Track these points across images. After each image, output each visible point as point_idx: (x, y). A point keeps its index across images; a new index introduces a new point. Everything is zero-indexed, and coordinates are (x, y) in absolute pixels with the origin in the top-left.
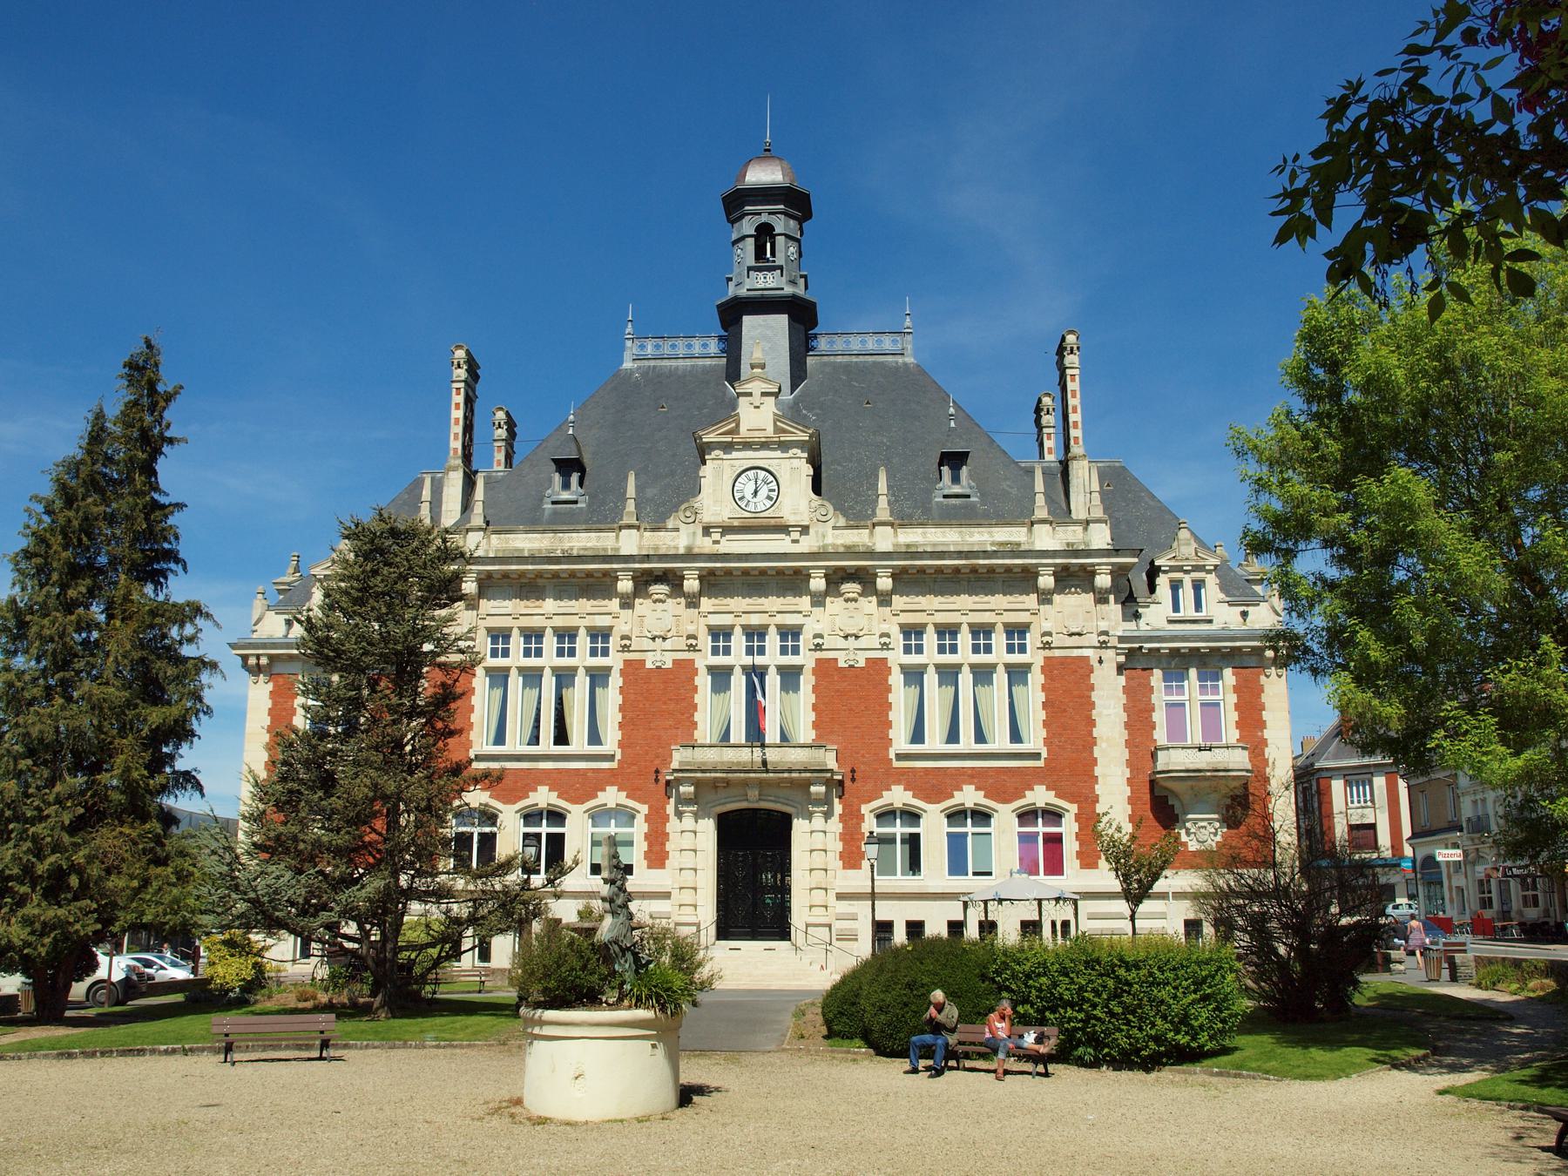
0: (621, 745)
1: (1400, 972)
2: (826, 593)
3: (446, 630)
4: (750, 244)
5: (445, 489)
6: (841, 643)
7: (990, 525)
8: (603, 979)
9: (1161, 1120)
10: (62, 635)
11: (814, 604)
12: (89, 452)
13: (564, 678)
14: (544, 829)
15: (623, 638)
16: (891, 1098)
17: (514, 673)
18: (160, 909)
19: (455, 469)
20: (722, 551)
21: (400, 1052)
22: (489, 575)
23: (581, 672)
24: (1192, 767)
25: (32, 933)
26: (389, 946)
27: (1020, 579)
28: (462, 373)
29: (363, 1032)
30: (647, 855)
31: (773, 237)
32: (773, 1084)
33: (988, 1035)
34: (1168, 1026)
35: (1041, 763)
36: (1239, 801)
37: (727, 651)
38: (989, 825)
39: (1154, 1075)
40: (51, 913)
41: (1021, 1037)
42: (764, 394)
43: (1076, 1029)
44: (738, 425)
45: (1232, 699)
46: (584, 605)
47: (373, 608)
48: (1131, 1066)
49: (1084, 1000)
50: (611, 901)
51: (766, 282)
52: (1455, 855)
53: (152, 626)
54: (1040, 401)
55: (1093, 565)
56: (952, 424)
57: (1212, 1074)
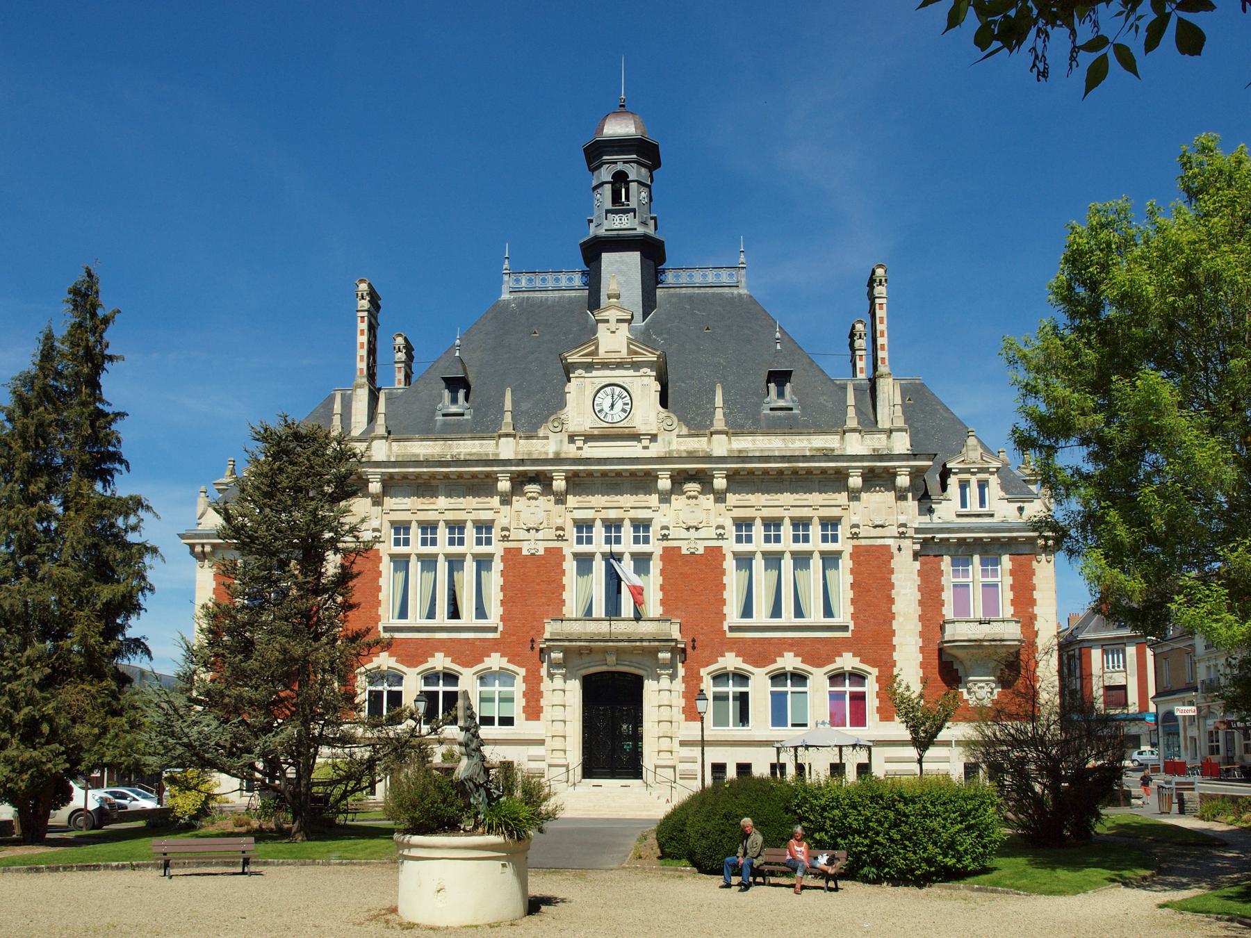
0: (502, 618)
1: (1138, 806)
2: (672, 492)
3: (342, 520)
4: (608, 188)
5: (354, 405)
6: (684, 534)
7: (809, 434)
8: (461, 810)
9: (925, 928)
10: (26, 524)
11: (661, 501)
12: (42, 368)
13: (455, 563)
14: (441, 688)
15: (503, 529)
16: (706, 908)
17: (413, 559)
18: (117, 752)
19: (361, 386)
20: (584, 456)
21: (309, 868)
22: (391, 476)
23: (469, 558)
24: (973, 637)
25: (13, 770)
26: (303, 782)
27: (834, 480)
28: (365, 304)
29: (280, 851)
30: (525, 709)
31: (627, 183)
32: (609, 896)
33: (789, 857)
34: (938, 850)
35: (848, 634)
36: (1012, 666)
37: (589, 540)
38: (805, 685)
39: (925, 890)
40: (27, 755)
41: (816, 858)
42: (619, 321)
43: (862, 853)
44: (597, 348)
45: (1009, 580)
46: (470, 502)
47: (280, 501)
48: (907, 883)
49: (869, 828)
50: (466, 745)
51: (622, 223)
52: (1191, 711)
53: (101, 517)
54: (853, 327)
55: (895, 467)
56: (779, 347)
57: (973, 890)
